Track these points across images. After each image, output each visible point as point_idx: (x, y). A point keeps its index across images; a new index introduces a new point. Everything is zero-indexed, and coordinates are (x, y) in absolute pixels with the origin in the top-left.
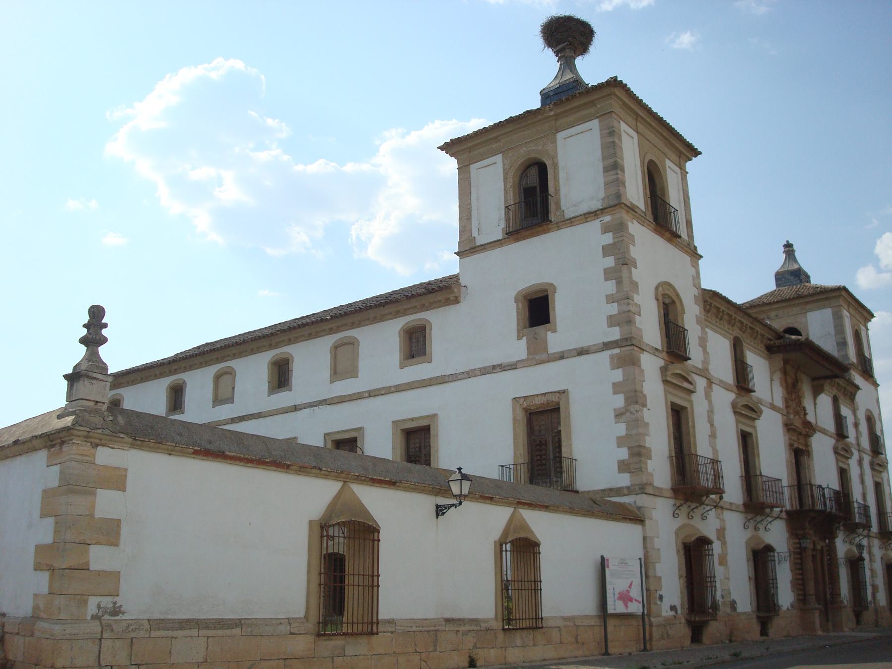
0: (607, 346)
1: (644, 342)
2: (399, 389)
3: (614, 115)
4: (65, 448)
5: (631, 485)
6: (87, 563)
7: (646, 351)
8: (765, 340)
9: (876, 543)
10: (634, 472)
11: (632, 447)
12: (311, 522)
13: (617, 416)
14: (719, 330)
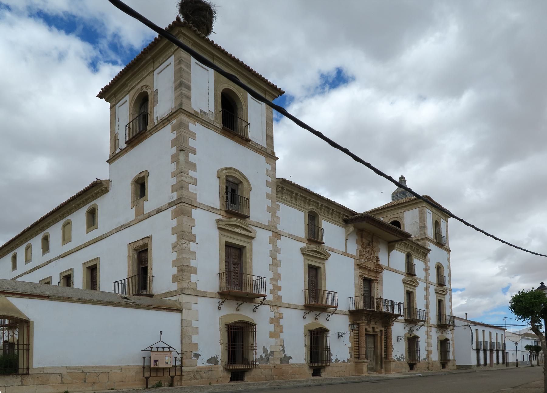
0: (170, 205)
8: (342, 216)
10: (179, 281)
11: (179, 266)
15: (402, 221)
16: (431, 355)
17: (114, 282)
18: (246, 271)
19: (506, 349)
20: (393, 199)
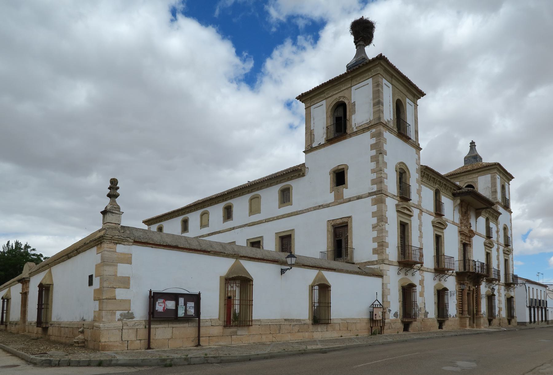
0: (370, 194)
1: (388, 192)
2: (278, 218)
3: (380, 76)
4: (102, 245)
5: (378, 260)
6: (115, 296)
7: (389, 196)
8: (452, 190)
9: (503, 288)
12: (221, 277)
13: (373, 227)
14: (428, 186)
15: (476, 186)
16: (501, 312)
17: (321, 252)
18: (408, 244)
19: (548, 307)
20: (466, 162)
